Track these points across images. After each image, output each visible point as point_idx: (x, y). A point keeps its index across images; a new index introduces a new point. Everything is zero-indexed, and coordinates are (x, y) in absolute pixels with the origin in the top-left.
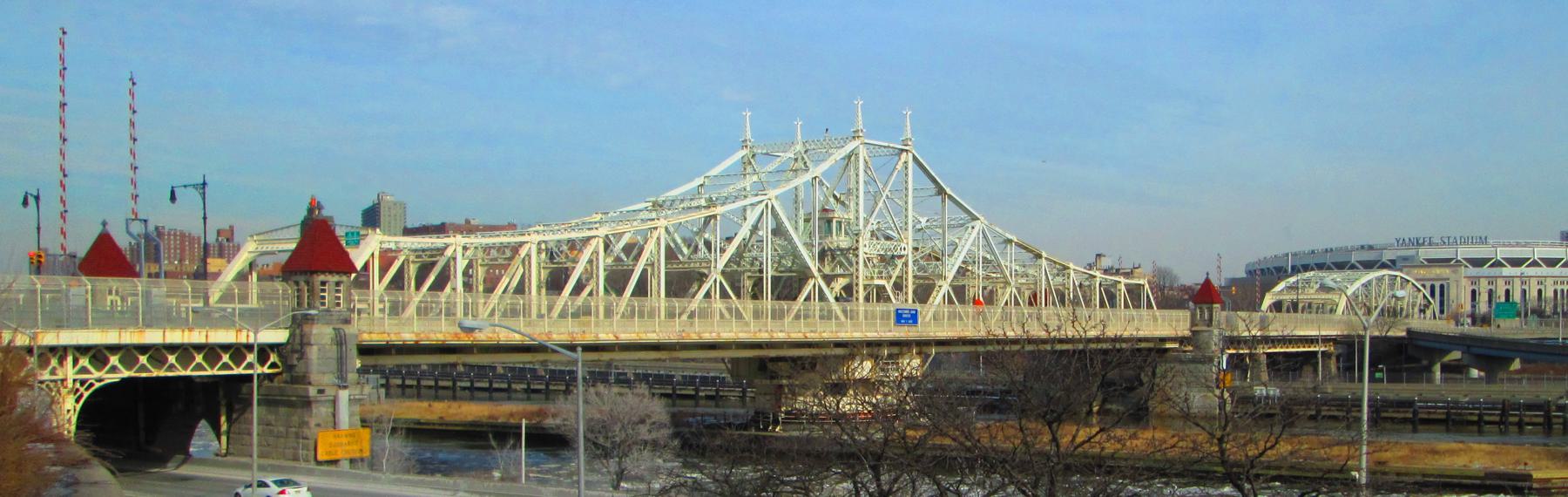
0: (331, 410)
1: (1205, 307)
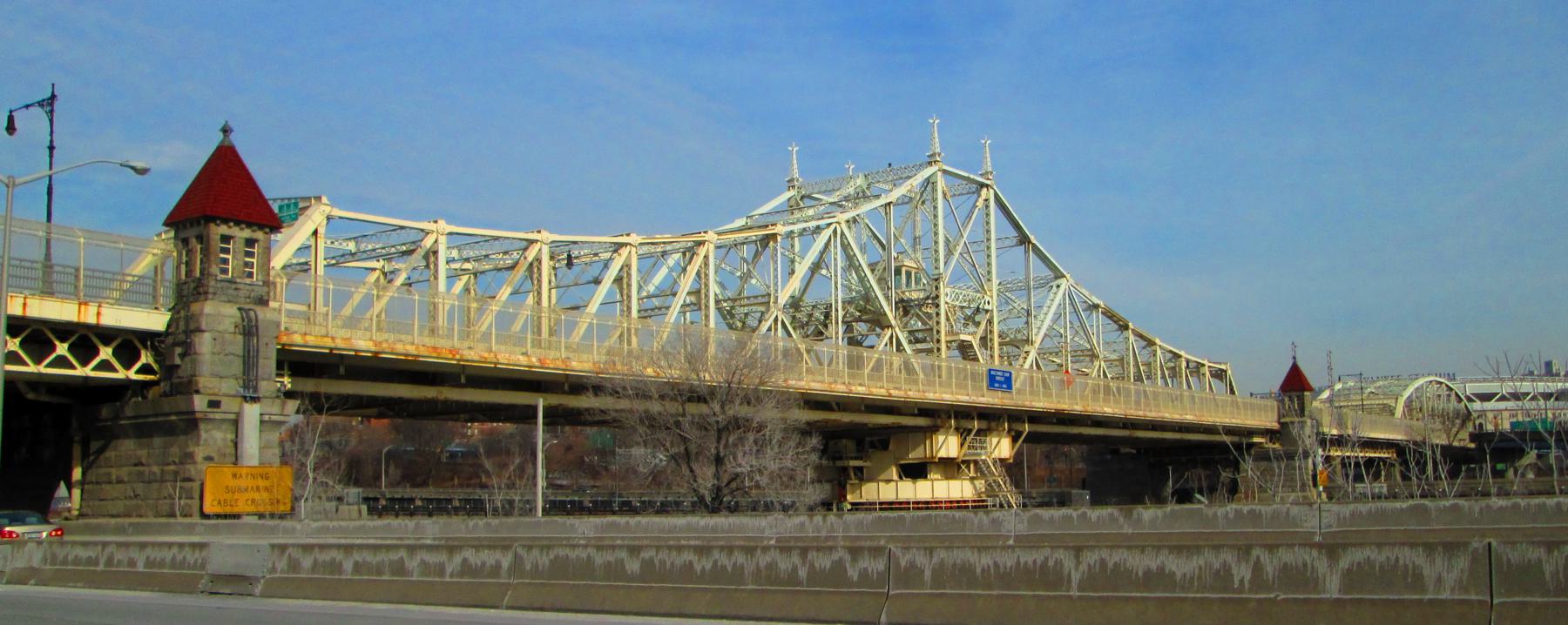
0: (231, 436)
1: (1294, 394)
